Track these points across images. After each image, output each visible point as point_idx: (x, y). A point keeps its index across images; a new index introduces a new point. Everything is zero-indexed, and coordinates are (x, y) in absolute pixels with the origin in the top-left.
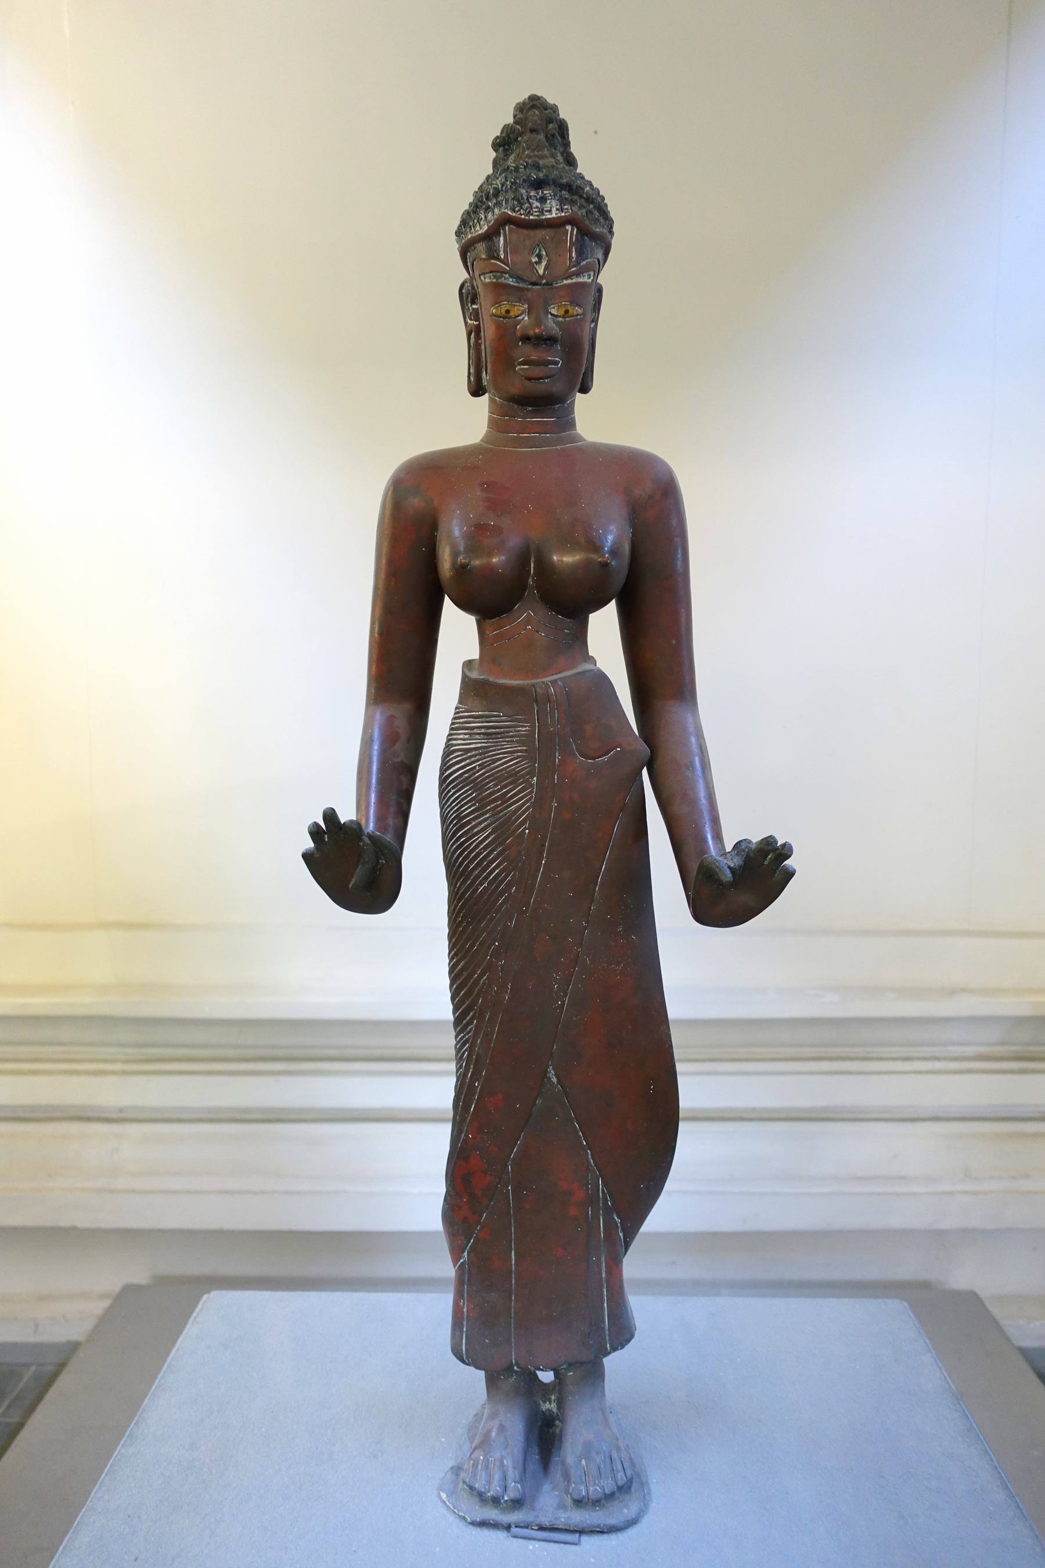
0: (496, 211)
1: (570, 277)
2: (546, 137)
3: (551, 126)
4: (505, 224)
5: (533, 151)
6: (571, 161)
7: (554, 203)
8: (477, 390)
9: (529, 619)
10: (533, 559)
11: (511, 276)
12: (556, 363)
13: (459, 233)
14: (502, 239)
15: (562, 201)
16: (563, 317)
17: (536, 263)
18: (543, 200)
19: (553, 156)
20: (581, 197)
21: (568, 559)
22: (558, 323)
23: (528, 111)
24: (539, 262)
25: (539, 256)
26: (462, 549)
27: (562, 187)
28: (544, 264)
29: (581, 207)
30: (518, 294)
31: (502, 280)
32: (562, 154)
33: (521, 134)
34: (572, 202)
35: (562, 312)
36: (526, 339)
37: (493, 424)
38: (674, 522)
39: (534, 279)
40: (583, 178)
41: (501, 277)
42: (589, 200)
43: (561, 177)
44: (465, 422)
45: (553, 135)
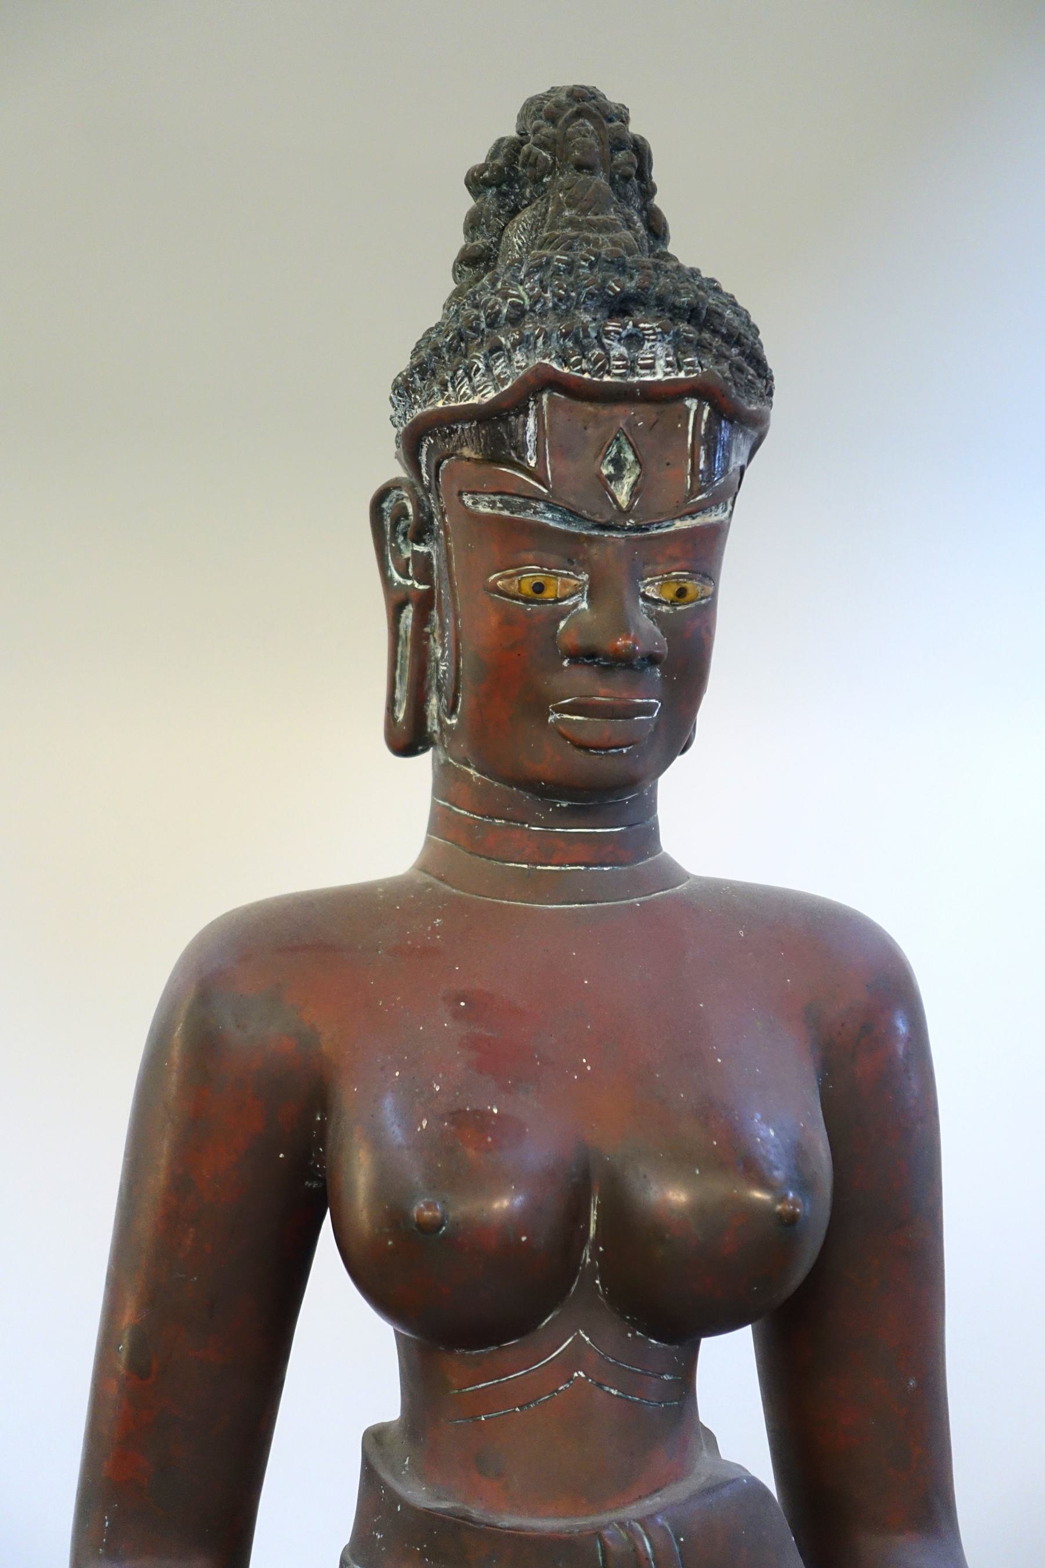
0: (518, 356)
1: (692, 514)
2: (612, 181)
3: (621, 156)
4: (542, 391)
5: (584, 212)
6: (656, 229)
7: (660, 350)
8: (407, 741)
9: (574, 1351)
10: (595, 1200)
11: (551, 508)
12: (648, 710)
13: (404, 388)
14: (531, 422)
15: (680, 345)
16: (672, 603)
17: (610, 478)
18: (634, 340)
19: (629, 224)
20: (715, 332)
21: (678, 1196)
22: (659, 619)
23: (568, 122)
24: (617, 477)
25: (618, 463)
26: (417, 1178)
27: (677, 313)
28: (628, 480)
29: (720, 357)
30: (570, 550)
31: (528, 516)
32: (640, 212)
33: (550, 171)
34: (701, 347)
35: (669, 593)
36: (585, 656)
37: (441, 823)
38: (914, 1085)
39: (606, 518)
40: (717, 290)
41: (523, 508)
42: (733, 338)
43: (676, 292)
44: (370, 819)
45: (627, 178)
